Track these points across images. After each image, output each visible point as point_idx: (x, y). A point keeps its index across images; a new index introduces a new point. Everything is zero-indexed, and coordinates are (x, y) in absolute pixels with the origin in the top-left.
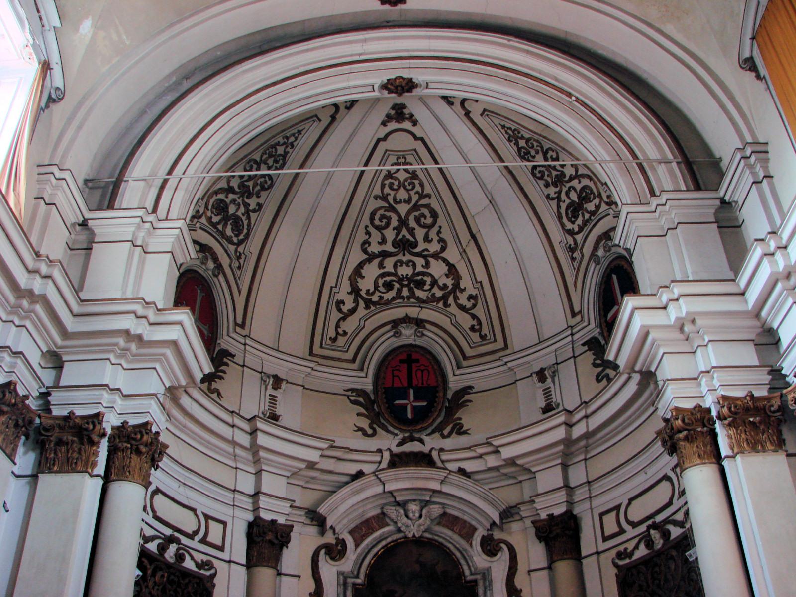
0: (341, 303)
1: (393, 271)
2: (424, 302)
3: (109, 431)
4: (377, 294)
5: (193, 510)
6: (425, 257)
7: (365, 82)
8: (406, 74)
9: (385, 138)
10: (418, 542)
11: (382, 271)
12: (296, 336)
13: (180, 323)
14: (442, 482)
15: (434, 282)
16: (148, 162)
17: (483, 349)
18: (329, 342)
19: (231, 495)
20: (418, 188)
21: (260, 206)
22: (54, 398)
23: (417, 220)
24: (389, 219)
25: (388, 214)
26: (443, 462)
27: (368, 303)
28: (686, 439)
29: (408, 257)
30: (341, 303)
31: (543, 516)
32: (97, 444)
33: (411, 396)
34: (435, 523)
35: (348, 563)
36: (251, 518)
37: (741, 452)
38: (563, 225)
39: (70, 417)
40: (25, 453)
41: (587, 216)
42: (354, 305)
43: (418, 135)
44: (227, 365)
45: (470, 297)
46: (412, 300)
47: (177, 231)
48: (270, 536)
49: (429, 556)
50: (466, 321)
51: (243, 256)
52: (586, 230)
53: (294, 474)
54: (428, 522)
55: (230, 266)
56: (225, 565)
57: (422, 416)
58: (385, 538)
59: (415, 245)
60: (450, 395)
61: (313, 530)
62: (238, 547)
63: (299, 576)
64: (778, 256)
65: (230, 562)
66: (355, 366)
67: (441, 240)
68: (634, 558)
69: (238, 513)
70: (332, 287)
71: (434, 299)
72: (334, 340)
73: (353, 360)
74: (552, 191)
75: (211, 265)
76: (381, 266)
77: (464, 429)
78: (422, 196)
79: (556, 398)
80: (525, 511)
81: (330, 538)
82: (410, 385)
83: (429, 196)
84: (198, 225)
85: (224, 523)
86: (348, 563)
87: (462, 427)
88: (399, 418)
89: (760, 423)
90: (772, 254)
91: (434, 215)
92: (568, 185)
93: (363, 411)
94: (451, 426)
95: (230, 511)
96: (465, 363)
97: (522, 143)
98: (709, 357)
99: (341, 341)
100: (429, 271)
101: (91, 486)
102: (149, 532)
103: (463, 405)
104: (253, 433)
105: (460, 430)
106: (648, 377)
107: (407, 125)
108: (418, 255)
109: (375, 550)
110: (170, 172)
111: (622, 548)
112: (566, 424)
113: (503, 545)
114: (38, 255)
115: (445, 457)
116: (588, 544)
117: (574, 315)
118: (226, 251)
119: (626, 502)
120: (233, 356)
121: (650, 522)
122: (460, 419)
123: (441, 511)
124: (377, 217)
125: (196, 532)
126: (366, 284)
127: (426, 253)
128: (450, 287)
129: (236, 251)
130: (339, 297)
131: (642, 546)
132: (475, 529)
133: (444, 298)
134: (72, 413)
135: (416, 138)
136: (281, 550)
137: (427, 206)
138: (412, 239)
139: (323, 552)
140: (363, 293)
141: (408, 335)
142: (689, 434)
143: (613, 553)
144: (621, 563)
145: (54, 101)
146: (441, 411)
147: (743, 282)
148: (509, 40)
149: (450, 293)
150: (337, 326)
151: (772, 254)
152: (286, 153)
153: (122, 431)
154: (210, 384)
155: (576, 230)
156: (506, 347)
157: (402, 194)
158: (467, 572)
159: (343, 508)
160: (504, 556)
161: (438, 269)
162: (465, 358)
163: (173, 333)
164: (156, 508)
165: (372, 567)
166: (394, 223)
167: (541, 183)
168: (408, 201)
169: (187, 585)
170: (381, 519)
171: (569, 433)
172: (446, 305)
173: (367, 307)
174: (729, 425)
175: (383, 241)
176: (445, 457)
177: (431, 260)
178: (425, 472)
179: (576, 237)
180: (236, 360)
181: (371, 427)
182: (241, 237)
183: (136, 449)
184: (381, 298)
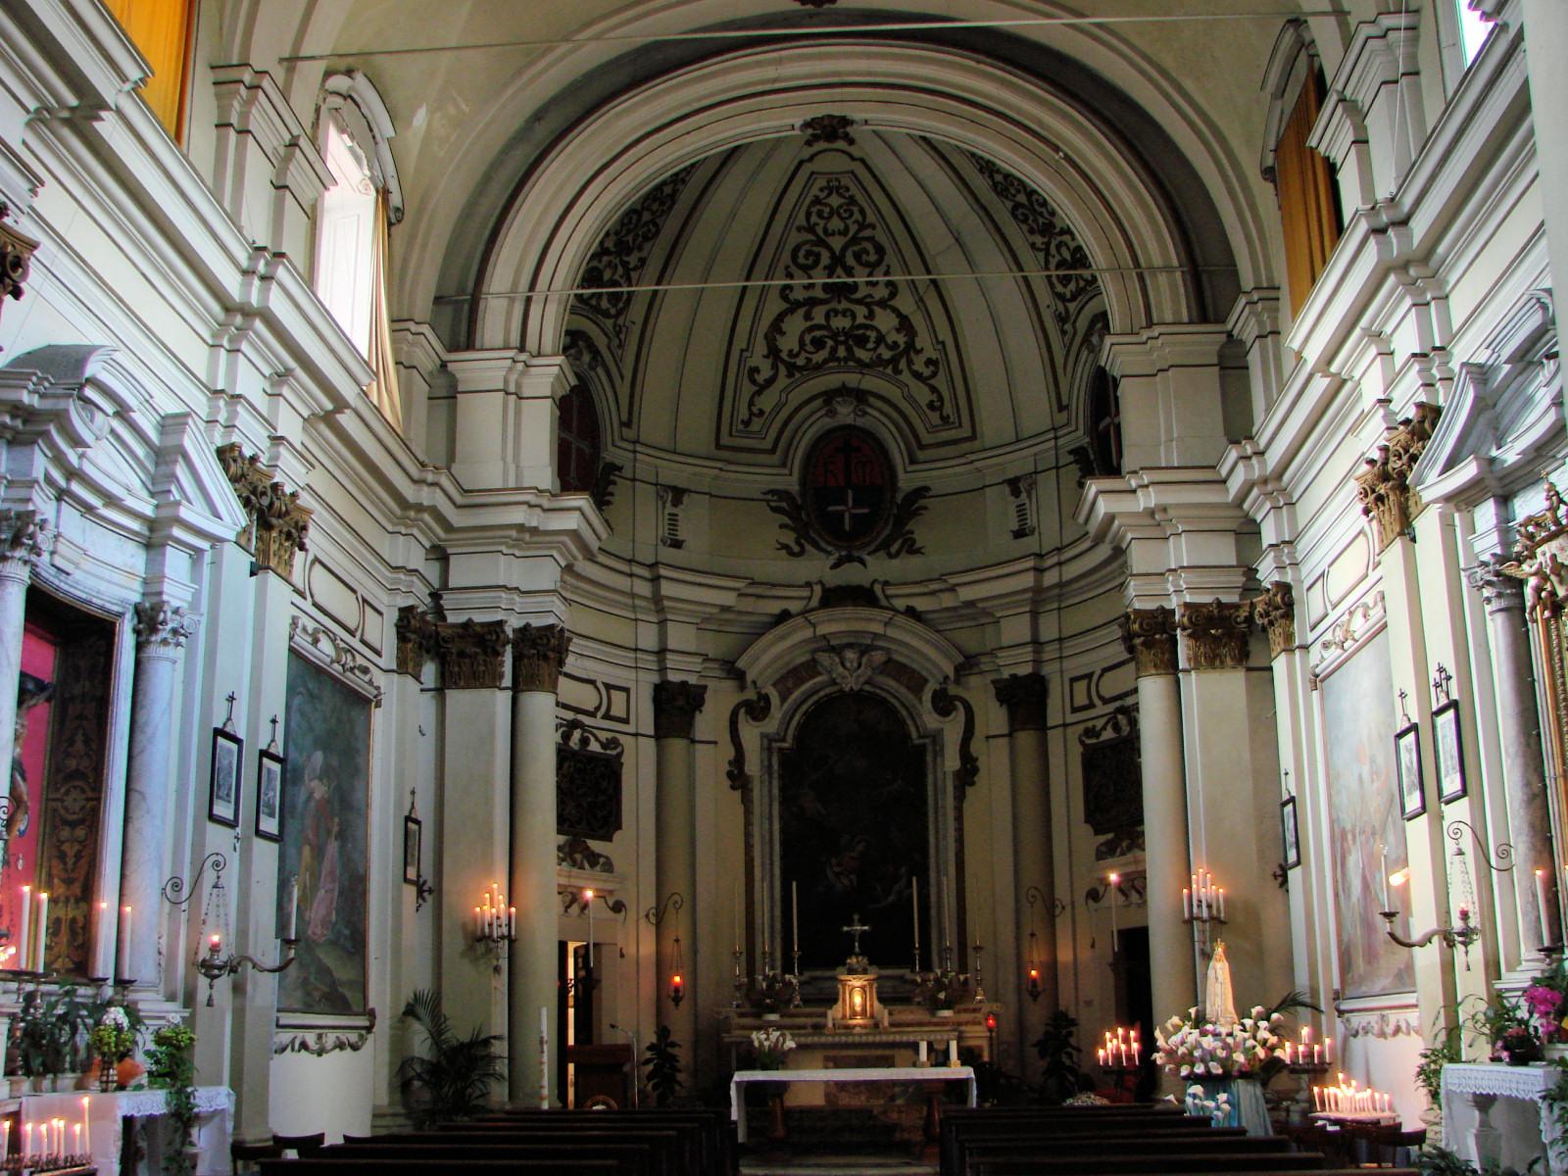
0: (755, 370)
1: (823, 322)
2: (867, 366)
4: (803, 355)
5: (592, 682)
6: (868, 305)
7: (786, 119)
8: (836, 110)
9: (811, 159)
10: (858, 696)
11: (809, 324)
12: (697, 429)
13: (579, 509)
14: (886, 624)
15: (881, 339)
17: (945, 435)
18: (741, 427)
19: (632, 655)
20: (857, 216)
21: (643, 261)
22: (448, 601)
23: (857, 256)
24: (818, 256)
25: (816, 249)
26: (887, 597)
27: (792, 369)
28: (1144, 644)
29: (844, 305)
31: (1006, 674)
32: (498, 654)
33: (849, 497)
35: (772, 725)
36: (655, 678)
37: (1196, 668)
38: (1052, 286)
41: (1082, 284)
42: (771, 373)
44: (614, 483)
45: (929, 362)
46: (851, 363)
47: (556, 369)
48: (681, 702)
50: (923, 395)
52: (1082, 299)
54: (869, 672)
55: (609, 348)
56: (631, 739)
58: (818, 691)
60: (899, 497)
61: (729, 685)
62: (644, 716)
63: (715, 743)
64: (1254, 460)
65: (636, 735)
66: (776, 458)
68: (1102, 738)
69: (642, 675)
70: (742, 351)
71: (879, 362)
72: (747, 423)
74: (1039, 240)
76: (808, 317)
77: (917, 545)
79: (1032, 521)
80: (986, 664)
81: (750, 694)
83: (873, 227)
85: (627, 690)
86: (772, 725)
87: (914, 541)
89: (1223, 635)
90: (1249, 458)
91: (880, 250)
92: (1059, 239)
93: (786, 520)
94: (899, 542)
95: (632, 674)
96: (921, 455)
97: (998, 178)
99: (757, 424)
100: (875, 323)
101: (502, 700)
103: (916, 513)
104: (655, 580)
105: (912, 549)
106: (1119, 552)
107: (841, 144)
108: (859, 302)
109: (804, 707)
110: (532, 288)
111: (1090, 724)
112: (1035, 569)
113: (958, 703)
114: (423, 465)
115: (890, 591)
116: (1055, 713)
117: (1062, 408)
118: (603, 330)
119: (1098, 672)
120: (620, 469)
121: (1118, 704)
122: (912, 533)
124: (801, 254)
125: (598, 708)
126: (788, 343)
128: (902, 346)
130: (752, 363)
131: (1109, 728)
132: (926, 681)
133: (894, 361)
134: (470, 620)
135: (853, 158)
136: (692, 718)
137: (871, 239)
139: (743, 710)
140: (784, 355)
141: (845, 413)
142: (1151, 637)
143: (1081, 728)
144: (1088, 741)
147: (1224, 472)
148: (978, 62)
149: (901, 355)
150: (751, 403)
151: (1249, 458)
152: (675, 192)
153: (524, 631)
155: (1068, 296)
156: (973, 437)
157: (836, 224)
158: (914, 735)
159: (765, 659)
160: (960, 715)
161: (885, 321)
162: (922, 447)
163: (571, 522)
165: (802, 728)
166: (825, 259)
167: (1025, 227)
168: (844, 232)
170: (811, 668)
171: (1038, 581)
173: (790, 375)
174: (1189, 636)
176: (890, 591)
177: (877, 309)
178: (866, 612)
179: (1069, 305)
181: (798, 543)
182: (621, 305)
183: (540, 653)
184: (809, 360)
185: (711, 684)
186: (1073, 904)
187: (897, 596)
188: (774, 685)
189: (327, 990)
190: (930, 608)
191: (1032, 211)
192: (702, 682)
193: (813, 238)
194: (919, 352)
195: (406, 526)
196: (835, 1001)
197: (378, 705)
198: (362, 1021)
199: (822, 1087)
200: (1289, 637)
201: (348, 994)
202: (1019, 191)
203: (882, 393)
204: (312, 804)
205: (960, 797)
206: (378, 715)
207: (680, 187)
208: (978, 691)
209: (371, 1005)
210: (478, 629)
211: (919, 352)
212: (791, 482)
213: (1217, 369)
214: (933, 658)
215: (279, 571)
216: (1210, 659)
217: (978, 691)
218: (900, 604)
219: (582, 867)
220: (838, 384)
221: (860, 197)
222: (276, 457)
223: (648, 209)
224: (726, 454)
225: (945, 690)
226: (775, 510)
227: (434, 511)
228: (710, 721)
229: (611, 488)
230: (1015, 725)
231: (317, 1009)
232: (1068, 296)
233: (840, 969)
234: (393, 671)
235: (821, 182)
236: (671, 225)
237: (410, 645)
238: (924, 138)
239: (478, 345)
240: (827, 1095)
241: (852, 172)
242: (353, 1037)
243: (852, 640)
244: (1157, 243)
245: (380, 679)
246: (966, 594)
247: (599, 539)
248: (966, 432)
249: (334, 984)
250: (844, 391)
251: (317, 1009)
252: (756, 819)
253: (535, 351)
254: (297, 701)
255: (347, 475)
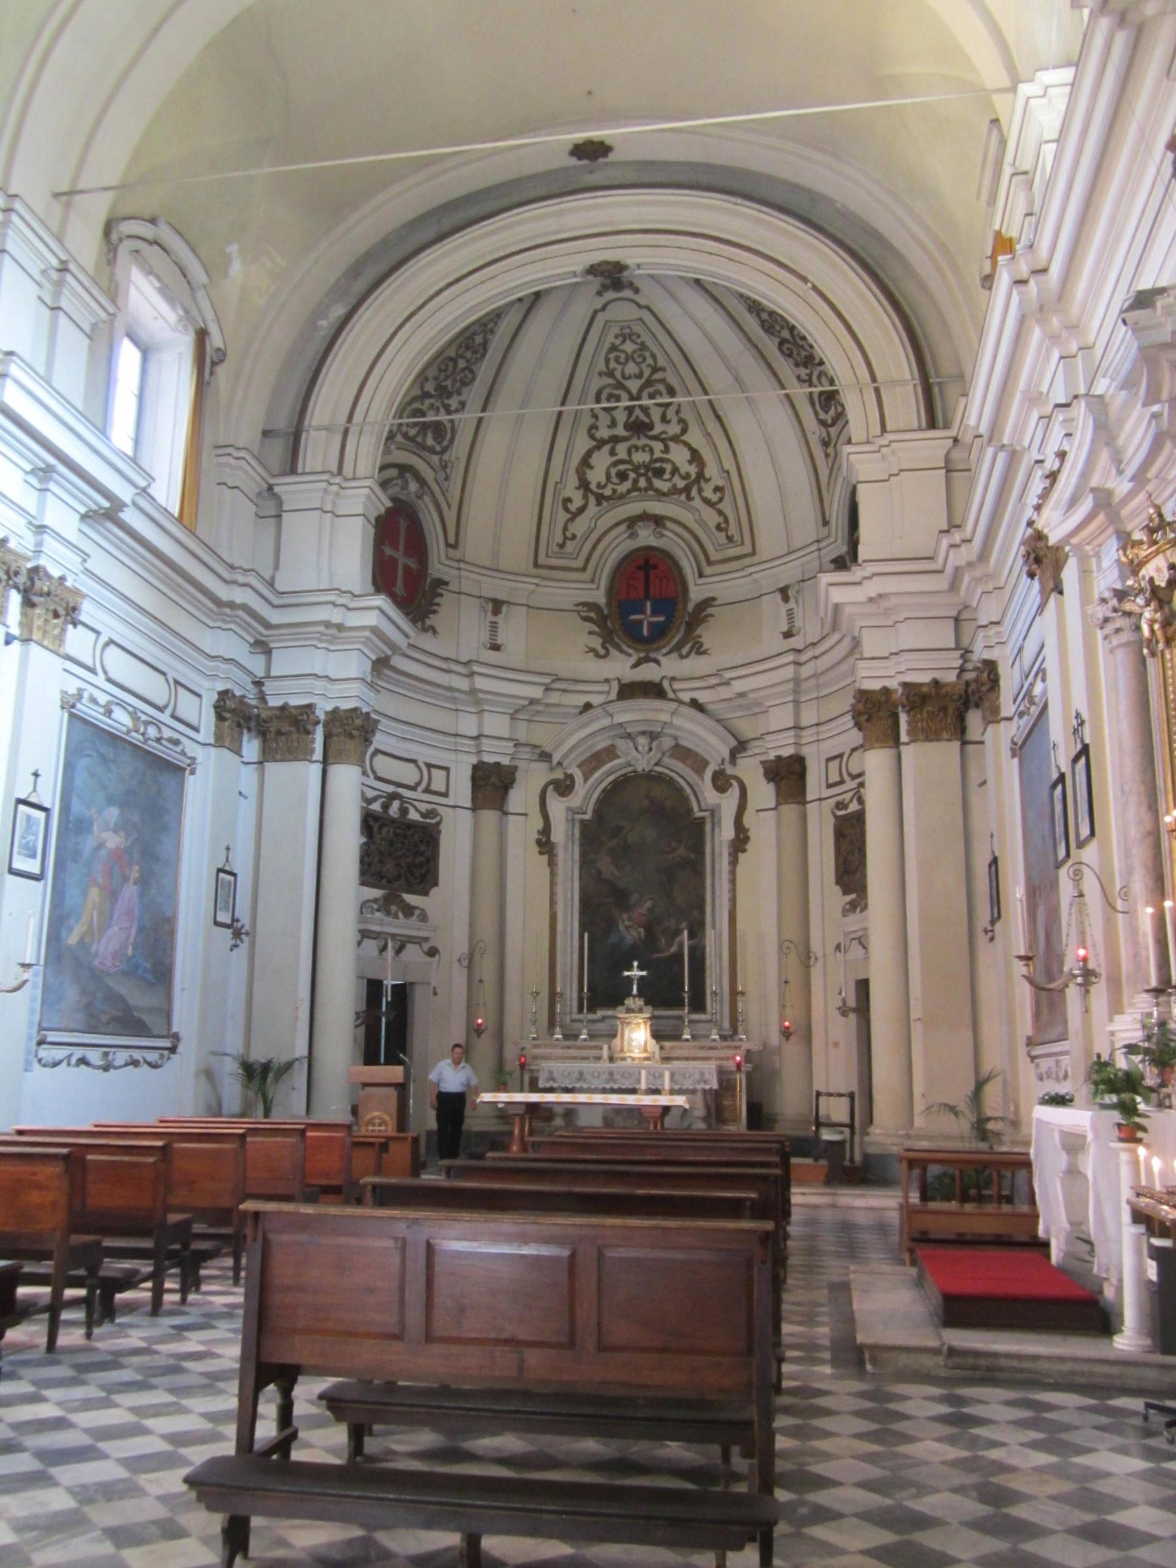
0: (567, 500)
1: (627, 458)
2: (664, 494)
3: (322, 717)
4: (610, 486)
5: (414, 761)
6: (663, 441)
7: (570, 263)
9: (604, 308)
10: (650, 777)
11: (614, 459)
14: (672, 714)
15: (675, 470)
16: (327, 406)
18: (556, 549)
20: (650, 361)
22: (268, 688)
25: (617, 392)
26: (674, 691)
27: (600, 499)
29: (643, 441)
30: (567, 500)
31: (772, 756)
32: (314, 733)
33: (648, 604)
34: (668, 754)
38: (816, 414)
39: (284, 708)
40: (249, 741)
43: (643, 303)
44: (441, 595)
45: (717, 489)
46: (650, 493)
49: (658, 791)
50: (712, 518)
51: (449, 465)
53: (517, 711)
55: (436, 480)
57: (659, 634)
59: (651, 426)
60: (690, 607)
62: (462, 790)
67: (681, 421)
68: (849, 811)
71: (675, 491)
72: (562, 546)
73: (584, 569)
74: (803, 372)
75: (413, 486)
76: (613, 453)
78: (655, 369)
79: (798, 623)
81: (559, 775)
82: (647, 597)
83: (663, 369)
84: (393, 447)
85: (447, 769)
86: (577, 799)
87: (701, 645)
88: (633, 635)
93: (596, 629)
94: (690, 644)
97: (765, 316)
98: (909, 636)
99: (570, 546)
101: (314, 771)
102: (371, 794)
103: (704, 620)
105: (699, 650)
107: (627, 293)
108: (655, 438)
109: (603, 786)
111: (840, 798)
113: (734, 782)
115: (676, 686)
116: (812, 791)
118: (429, 464)
120: (446, 583)
122: (700, 637)
123: (673, 743)
125: (418, 784)
126: (596, 476)
127: (664, 436)
128: (694, 476)
129: (441, 460)
131: (855, 801)
133: (687, 489)
135: (639, 306)
137: (662, 381)
138: (646, 420)
139: (551, 787)
140: (593, 487)
141: (646, 537)
143: (832, 801)
145: (217, 364)
146: (679, 626)
149: (693, 484)
150: (565, 529)
154: (423, 623)
155: (830, 422)
156: (754, 553)
157: (631, 368)
160: (735, 792)
161: (679, 455)
162: (709, 563)
164: (376, 769)
167: (791, 361)
168: (640, 376)
169: (412, 835)
170: (610, 752)
172: (689, 498)
173: (599, 504)
175: (613, 424)
176: (676, 686)
177: (671, 444)
180: (451, 587)
181: (604, 647)
183: (351, 732)
184: (614, 491)
185: (522, 765)
186: (825, 955)
187: (681, 690)
188: (579, 766)
189: (119, 1014)
190: (710, 699)
191: (796, 348)
192: (513, 763)
193: (611, 381)
194: (708, 480)
195: (224, 621)
196: (614, 1036)
197: (193, 773)
198: (167, 1043)
199: (600, 1110)
200: (996, 710)
201: (147, 1019)
202: (782, 327)
203: (680, 519)
204: (103, 852)
205: (734, 862)
206: (192, 785)
207: (489, 336)
208: (750, 770)
209: (175, 1029)
210: (294, 711)
211: (708, 480)
212: (599, 596)
213: (944, 471)
214: (715, 747)
215: (46, 643)
216: (926, 733)
217: (750, 770)
218: (686, 697)
219: (396, 917)
220: (639, 512)
221: (650, 343)
222: (40, 544)
223: (462, 356)
224: (544, 572)
225: (724, 770)
226: (586, 619)
227: (246, 608)
228: (522, 797)
229: (437, 600)
230: (783, 797)
231: (103, 1029)
232: (830, 422)
233: (620, 1008)
234: (209, 745)
235: (615, 330)
236: (485, 371)
237: (227, 723)
238: (697, 281)
239: (300, 470)
240: (605, 1118)
241: (641, 319)
242: (153, 1056)
243: (645, 728)
244: (895, 362)
245: (192, 749)
246: (738, 686)
247: (407, 636)
248: (747, 549)
249: (128, 1009)
250: (645, 517)
251: (103, 1029)
252: (560, 879)
253: (350, 476)
254: (83, 763)
255: (149, 571)
